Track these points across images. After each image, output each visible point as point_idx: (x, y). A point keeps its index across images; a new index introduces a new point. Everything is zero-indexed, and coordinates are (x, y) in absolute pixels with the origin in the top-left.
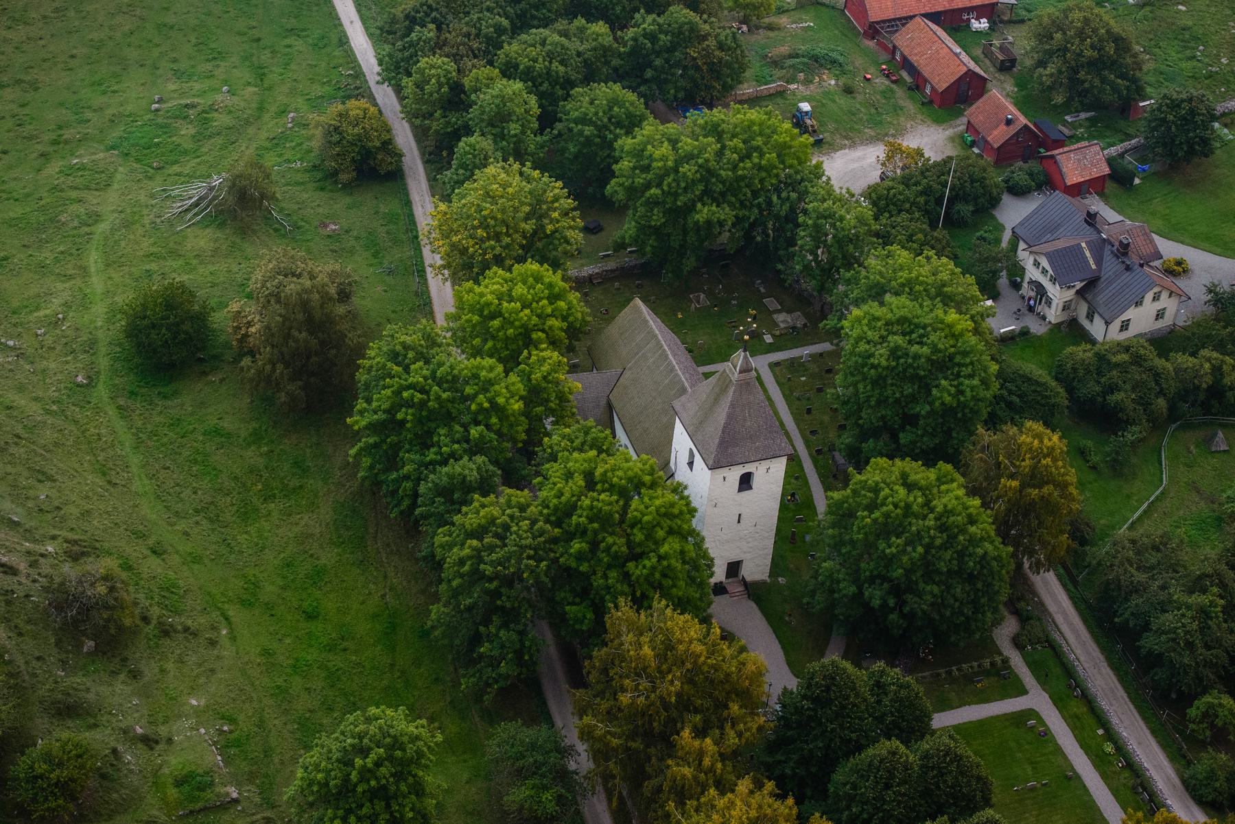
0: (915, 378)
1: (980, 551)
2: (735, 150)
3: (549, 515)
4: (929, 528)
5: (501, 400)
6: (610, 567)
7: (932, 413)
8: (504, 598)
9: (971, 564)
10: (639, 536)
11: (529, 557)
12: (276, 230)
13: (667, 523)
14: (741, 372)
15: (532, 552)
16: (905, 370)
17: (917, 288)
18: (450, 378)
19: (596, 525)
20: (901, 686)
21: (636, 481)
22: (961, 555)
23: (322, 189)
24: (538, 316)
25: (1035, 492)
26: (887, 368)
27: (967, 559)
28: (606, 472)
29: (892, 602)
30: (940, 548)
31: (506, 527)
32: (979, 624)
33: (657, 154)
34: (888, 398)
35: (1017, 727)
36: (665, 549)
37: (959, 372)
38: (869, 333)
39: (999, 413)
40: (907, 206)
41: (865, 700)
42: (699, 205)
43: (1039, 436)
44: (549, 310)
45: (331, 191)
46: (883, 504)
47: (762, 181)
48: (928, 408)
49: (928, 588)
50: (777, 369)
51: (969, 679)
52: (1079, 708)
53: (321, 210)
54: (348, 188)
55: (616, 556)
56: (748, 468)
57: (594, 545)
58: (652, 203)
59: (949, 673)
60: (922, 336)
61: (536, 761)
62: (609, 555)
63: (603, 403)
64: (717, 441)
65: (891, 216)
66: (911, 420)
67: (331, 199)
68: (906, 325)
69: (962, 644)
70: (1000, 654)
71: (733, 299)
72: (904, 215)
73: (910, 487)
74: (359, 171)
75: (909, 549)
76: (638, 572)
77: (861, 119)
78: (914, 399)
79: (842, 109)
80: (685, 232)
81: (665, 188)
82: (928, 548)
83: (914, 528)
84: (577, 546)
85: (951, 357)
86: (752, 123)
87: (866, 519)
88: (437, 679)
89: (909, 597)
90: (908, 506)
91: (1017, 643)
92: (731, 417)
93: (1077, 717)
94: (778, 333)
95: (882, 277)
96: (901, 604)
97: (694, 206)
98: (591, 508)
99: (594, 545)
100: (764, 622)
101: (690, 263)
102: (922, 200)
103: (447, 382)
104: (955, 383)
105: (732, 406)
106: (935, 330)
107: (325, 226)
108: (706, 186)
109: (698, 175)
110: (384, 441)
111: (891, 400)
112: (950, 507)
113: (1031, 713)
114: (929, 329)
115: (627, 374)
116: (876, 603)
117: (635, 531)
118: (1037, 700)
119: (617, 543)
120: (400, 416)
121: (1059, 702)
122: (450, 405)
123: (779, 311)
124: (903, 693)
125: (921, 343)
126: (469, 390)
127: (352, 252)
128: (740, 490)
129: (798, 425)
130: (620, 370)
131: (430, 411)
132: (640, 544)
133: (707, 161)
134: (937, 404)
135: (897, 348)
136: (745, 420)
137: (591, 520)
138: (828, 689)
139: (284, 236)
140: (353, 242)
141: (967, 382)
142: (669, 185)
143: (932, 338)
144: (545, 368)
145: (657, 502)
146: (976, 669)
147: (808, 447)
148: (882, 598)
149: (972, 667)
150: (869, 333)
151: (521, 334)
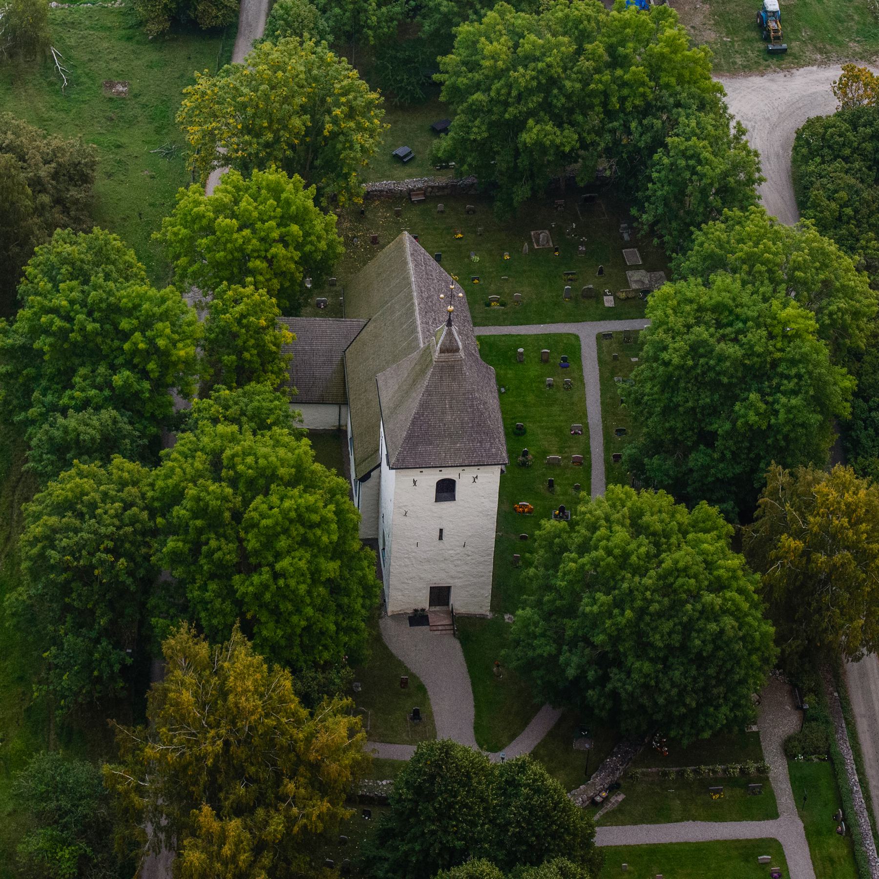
0: (716, 385)
1: (713, 627)
2: (594, 57)
3: (153, 499)
4: (647, 589)
5: (161, 343)
6: (212, 576)
7: (731, 434)
8: (74, 595)
9: (697, 642)
10: (252, 543)
11: (107, 551)
12: (51, 84)
13: (297, 530)
14: (442, 351)
15: (111, 544)
16: (704, 373)
17: (758, 267)
18: (103, 305)
19: (199, 523)
20: (537, 791)
21: (268, 472)
22: (688, 628)
23: (129, 39)
24: (262, 240)
25: (821, 558)
26: (681, 367)
27: (694, 634)
28: (234, 456)
29: (591, 675)
30: (660, 615)
31: (93, 506)
32: (710, 721)
33: (489, 48)
34: (678, 405)
35: (747, 860)
36: (283, 564)
37: (779, 385)
38: (672, 318)
39: (864, 441)
40: (847, 152)
41: (483, 800)
42: (531, 122)
43: (843, 488)
44: (275, 235)
45: (138, 43)
46: (596, 548)
47: (623, 100)
48: (728, 426)
49: (638, 664)
50: (606, 342)
51: (705, 786)
52: (836, 848)
53: (115, 66)
54: (160, 40)
55: (220, 565)
56: (449, 474)
57: (196, 548)
58: (474, 111)
59: (681, 774)
60: (739, 332)
61: (59, 808)
62: (211, 562)
63: (337, 360)
64: (404, 434)
65: (823, 162)
66: (708, 439)
67: (134, 52)
68: (724, 316)
69: (685, 742)
70: (760, 758)
71: (582, 244)
72: (838, 164)
73: (637, 527)
74: (175, 20)
75: (616, 611)
76: (242, 589)
77: (848, 29)
78: (714, 411)
79: (827, 12)
80: (517, 154)
81: (493, 94)
82: (642, 612)
83: (625, 585)
84: (172, 543)
85: (775, 364)
86: (626, 24)
87: (571, 563)
88: (21, 678)
89: (614, 673)
90: (626, 555)
91: (788, 751)
92: (424, 405)
93: (832, 861)
94: (623, 296)
95: (721, 247)
96: (604, 679)
97: (525, 122)
98: (198, 499)
99: (196, 548)
100: (464, 669)
101: (522, 192)
102: (868, 146)
103: (100, 310)
104: (770, 399)
105: (428, 392)
106: (758, 326)
107: (111, 85)
108: (545, 98)
109: (535, 83)
110: (19, 372)
111: (681, 409)
112: (681, 565)
113: (773, 846)
114: (750, 323)
115: (370, 327)
116: (571, 672)
117: (250, 536)
118: (787, 830)
119: (227, 551)
120: (37, 345)
121: (814, 835)
122: (99, 340)
123: (637, 267)
124: (536, 800)
125: (735, 340)
126: (125, 324)
127: (131, 123)
128: (438, 499)
129: (604, 419)
130: (363, 321)
131: (75, 344)
132: (256, 552)
133: (549, 66)
134: (739, 423)
135: (704, 343)
136: (444, 413)
137: (195, 515)
138: (432, 777)
139: (57, 92)
140: (138, 111)
141: (784, 400)
142: (498, 92)
143: (749, 335)
144: (241, 307)
145: (287, 504)
146: (720, 774)
147: (607, 449)
148: (579, 666)
149: (714, 772)
150: (672, 318)
151: (234, 259)
